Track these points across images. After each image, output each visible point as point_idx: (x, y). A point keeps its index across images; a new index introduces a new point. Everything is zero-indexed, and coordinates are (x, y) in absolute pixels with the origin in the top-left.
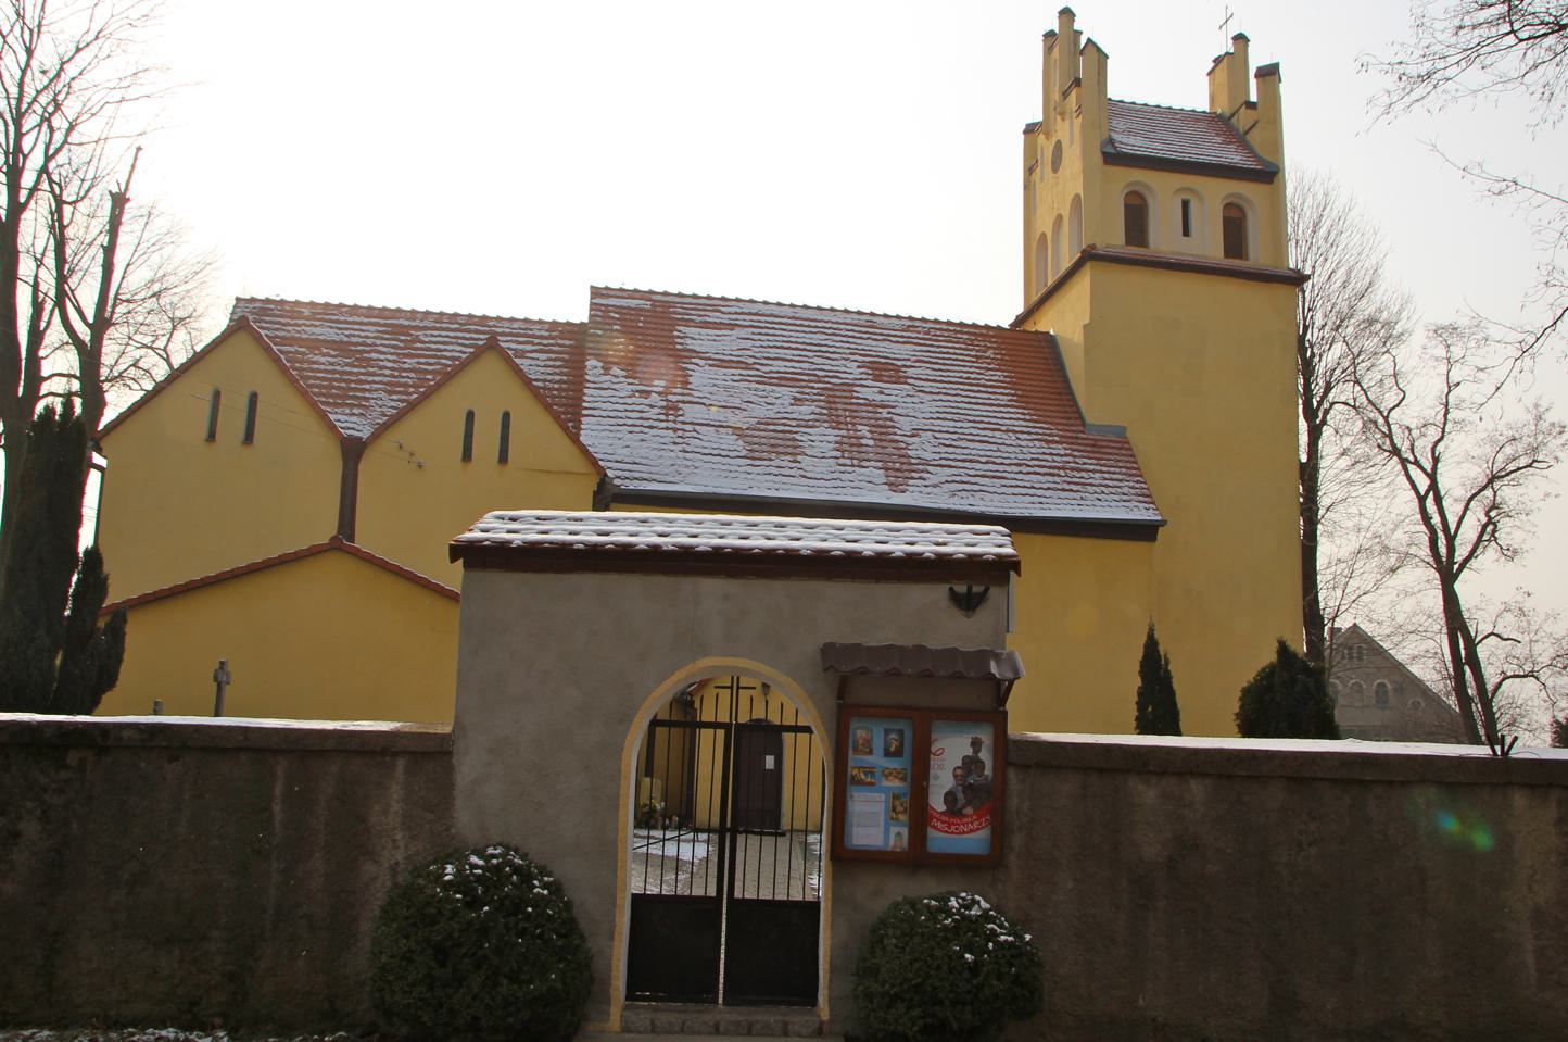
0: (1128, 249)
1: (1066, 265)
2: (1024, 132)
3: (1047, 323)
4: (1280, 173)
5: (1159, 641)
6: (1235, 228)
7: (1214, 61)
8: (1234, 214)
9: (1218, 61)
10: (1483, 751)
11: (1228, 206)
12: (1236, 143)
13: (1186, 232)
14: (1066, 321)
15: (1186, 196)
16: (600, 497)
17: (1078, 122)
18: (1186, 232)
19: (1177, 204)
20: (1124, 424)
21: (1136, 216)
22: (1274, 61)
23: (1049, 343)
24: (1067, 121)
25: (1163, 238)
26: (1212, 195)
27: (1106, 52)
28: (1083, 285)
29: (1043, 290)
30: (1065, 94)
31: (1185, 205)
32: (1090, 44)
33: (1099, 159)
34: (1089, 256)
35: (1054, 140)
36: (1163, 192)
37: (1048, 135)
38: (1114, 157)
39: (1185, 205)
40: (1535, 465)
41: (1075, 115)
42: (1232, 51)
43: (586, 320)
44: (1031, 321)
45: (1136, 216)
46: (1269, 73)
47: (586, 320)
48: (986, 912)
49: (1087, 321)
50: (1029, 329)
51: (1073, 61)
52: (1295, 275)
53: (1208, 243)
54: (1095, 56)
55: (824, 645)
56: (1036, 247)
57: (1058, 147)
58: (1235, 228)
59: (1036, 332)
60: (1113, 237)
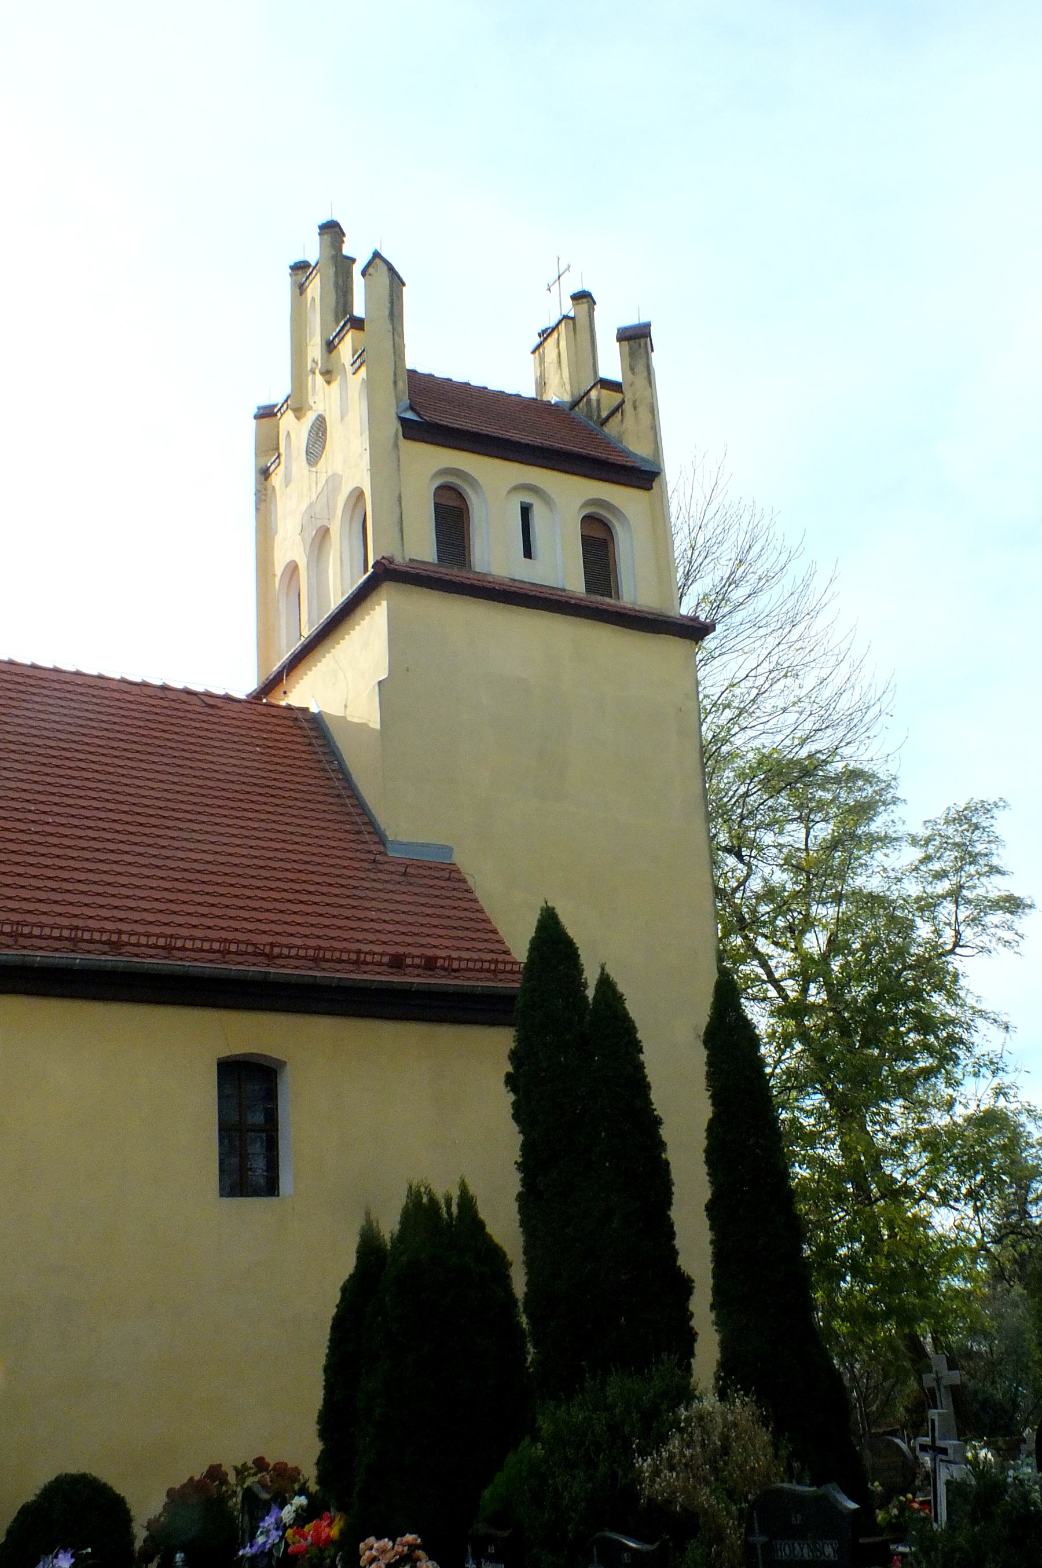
0: (442, 569)
1: (335, 600)
2: (256, 417)
3: (305, 693)
4: (660, 477)
5: (82, 1471)
6: (598, 544)
7: (539, 335)
8: (598, 533)
9: (545, 334)
11: (589, 520)
12: (589, 440)
13: (528, 553)
14: (343, 688)
15: (528, 498)
18: (528, 553)
19: (526, 485)
20: (450, 844)
21: (452, 516)
22: (644, 320)
23: (312, 728)
24: (335, 385)
25: (493, 553)
26: (568, 496)
27: (404, 280)
28: (374, 623)
29: (297, 646)
30: (330, 346)
31: (526, 511)
32: (377, 260)
33: (395, 426)
34: (384, 575)
35: (310, 417)
36: (496, 486)
37: (299, 412)
38: (415, 430)
39: (526, 511)
40: (958, 950)
41: (350, 370)
42: (572, 314)
44: (278, 692)
45: (452, 516)
46: (636, 339)
49: (384, 675)
50: (274, 702)
51: (347, 294)
52: (690, 623)
53: (561, 567)
54: (384, 278)
56: (274, 586)
57: (320, 429)
58: (598, 544)
59: (289, 708)
60: (422, 546)
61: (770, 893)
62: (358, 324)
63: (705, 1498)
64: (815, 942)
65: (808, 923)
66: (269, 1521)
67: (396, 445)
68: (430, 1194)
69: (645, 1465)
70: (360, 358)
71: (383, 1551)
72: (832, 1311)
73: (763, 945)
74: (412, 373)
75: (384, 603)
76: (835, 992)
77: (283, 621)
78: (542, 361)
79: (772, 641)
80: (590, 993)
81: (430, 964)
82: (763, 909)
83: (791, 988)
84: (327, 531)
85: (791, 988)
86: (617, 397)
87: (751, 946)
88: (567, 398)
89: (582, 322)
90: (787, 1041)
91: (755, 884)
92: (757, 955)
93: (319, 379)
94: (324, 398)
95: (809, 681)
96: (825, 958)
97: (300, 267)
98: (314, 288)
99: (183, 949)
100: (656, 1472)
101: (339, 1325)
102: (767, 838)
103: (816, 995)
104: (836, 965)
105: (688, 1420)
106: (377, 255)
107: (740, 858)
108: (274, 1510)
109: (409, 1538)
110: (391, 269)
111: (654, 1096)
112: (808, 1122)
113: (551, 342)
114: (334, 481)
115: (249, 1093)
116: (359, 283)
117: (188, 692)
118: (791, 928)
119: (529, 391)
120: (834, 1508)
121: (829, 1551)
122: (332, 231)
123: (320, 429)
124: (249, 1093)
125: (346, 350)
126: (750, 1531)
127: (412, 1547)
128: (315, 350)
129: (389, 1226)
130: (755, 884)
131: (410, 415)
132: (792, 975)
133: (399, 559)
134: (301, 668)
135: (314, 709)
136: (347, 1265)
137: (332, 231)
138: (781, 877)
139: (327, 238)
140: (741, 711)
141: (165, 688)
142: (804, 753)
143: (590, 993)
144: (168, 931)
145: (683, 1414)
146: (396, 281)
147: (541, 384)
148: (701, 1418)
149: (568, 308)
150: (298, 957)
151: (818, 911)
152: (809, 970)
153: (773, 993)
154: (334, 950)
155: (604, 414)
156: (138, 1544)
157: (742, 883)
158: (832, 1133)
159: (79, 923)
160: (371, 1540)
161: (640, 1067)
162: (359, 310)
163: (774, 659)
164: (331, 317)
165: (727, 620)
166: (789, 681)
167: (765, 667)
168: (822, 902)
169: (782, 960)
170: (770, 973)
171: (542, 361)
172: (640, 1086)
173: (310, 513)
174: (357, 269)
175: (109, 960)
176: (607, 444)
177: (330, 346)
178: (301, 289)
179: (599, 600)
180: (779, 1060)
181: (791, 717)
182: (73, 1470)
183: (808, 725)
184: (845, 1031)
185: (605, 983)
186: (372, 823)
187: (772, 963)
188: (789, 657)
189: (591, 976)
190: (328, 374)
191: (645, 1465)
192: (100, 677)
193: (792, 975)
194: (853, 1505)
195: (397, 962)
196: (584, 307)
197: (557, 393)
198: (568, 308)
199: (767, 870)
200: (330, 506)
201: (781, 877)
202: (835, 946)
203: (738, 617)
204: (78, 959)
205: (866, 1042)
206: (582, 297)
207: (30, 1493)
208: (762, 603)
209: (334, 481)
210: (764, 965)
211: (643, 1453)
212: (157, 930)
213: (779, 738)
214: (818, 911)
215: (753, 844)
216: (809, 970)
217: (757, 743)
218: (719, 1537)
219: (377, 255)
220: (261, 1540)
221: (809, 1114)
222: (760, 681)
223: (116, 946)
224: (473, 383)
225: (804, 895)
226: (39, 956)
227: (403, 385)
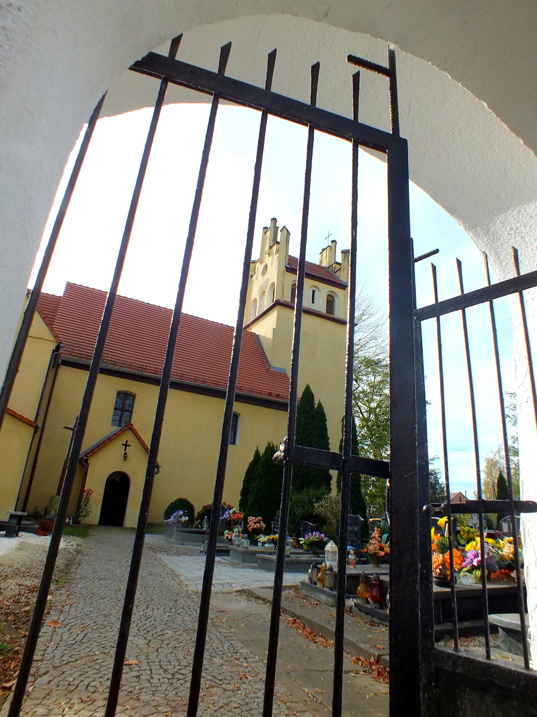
1: (265, 308)
6: (330, 302)
8: (331, 299)
9: (323, 250)
10: (12, 694)
13: (313, 302)
15: (314, 289)
16: (56, 353)
17: (276, 257)
18: (313, 302)
23: (256, 337)
24: (271, 257)
26: (324, 289)
28: (273, 316)
30: (271, 247)
31: (314, 292)
34: (277, 304)
35: (264, 264)
37: (261, 263)
39: (314, 292)
41: (275, 254)
43: (62, 296)
47: (62, 296)
48: (448, 522)
53: (321, 306)
55: (405, 141)
58: (330, 302)
59: (251, 332)
61: (363, 392)
62: (278, 243)
63: (329, 514)
64: (373, 405)
65: (372, 400)
66: (227, 513)
67: (284, 273)
68: (273, 444)
69: (316, 505)
70: (277, 251)
71: (253, 520)
72: (366, 494)
73: (360, 404)
74: (99, 523)
75: (276, 312)
76: (377, 416)
77: (252, 312)
78: (322, 256)
79: (371, 330)
80: (316, 406)
81: (278, 396)
82: (361, 395)
83: (366, 415)
84: (265, 292)
85: (366, 415)
86: (340, 267)
87: (357, 404)
88: (327, 266)
89: (333, 247)
90: (363, 427)
91: (360, 389)
92: (358, 406)
93: (267, 255)
94: (268, 260)
95: (380, 341)
96: (375, 408)
97: (265, 228)
98: (268, 233)
99: (220, 385)
100: (318, 507)
101: (248, 472)
102: (364, 378)
103: (372, 417)
104: (378, 410)
105: (327, 498)
106: (284, 227)
107: (357, 382)
108: (228, 510)
109: (259, 518)
110: (287, 230)
111: (328, 432)
112: (366, 447)
113: (325, 251)
114: (268, 280)
115: (231, 423)
116: (279, 233)
117: (227, 326)
118: (368, 401)
119: (318, 263)
120: (359, 519)
121: (356, 529)
122: (274, 220)
123: (266, 267)
124: (231, 423)
125: (274, 248)
126: (338, 523)
127: (260, 520)
128: (267, 248)
129: (262, 451)
130: (360, 389)
131: (288, 266)
132: (367, 411)
133: (281, 300)
134: (255, 324)
135: (257, 333)
136: (251, 458)
137: (274, 220)
138: (366, 388)
139: (273, 222)
140: (362, 346)
141: (222, 324)
142: (376, 358)
143: (316, 406)
144: (217, 380)
145: (326, 496)
146: (288, 233)
147: (321, 262)
148: (330, 498)
149: (330, 244)
150: (246, 390)
151: (375, 397)
152: (371, 411)
153: (361, 416)
154: (255, 390)
155: (336, 270)
156: (196, 516)
157: (357, 389)
158: (371, 451)
159: (197, 376)
160: (251, 517)
161: (326, 425)
162: (278, 240)
163: (372, 334)
164: (272, 240)
165: (361, 324)
166: (374, 340)
167: (369, 336)
168: (376, 395)
169: (364, 408)
170: (361, 411)
171: (322, 256)
172: (325, 429)
173: (261, 287)
174: (279, 230)
175: (203, 385)
176: (336, 278)
177: (271, 247)
178: (265, 233)
179: (329, 315)
180: (361, 432)
181: (374, 349)
182: (183, 497)
183: (378, 352)
184: (378, 426)
185: (320, 404)
186: (268, 362)
187: (362, 408)
188: (374, 334)
189: (316, 402)
190: (269, 254)
191: (316, 505)
192: (207, 320)
193: (367, 411)
194: (362, 519)
195: (270, 394)
196: (334, 244)
197: (325, 264)
198: (330, 244)
199: (363, 385)
200: (266, 286)
201: (366, 388)
202: (378, 406)
203: (364, 323)
204: (195, 384)
205: (383, 430)
206: (334, 242)
207: (173, 500)
208: (370, 320)
209: (268, 280)
210: (360, 409)
211: (316, 503)
212: (214, 380)
213: (370, 354)
214: (375, 397)
215: (361, 380)
216: (371, 411)
217: (364, 355)
218: (331, 524)
219: (284, 227)
220: (225, 516)
221: (366, 445)
222: (367, 339)
223: (204, 382)
224: (107, 118)
225: (373, 393)
226: (186, 382)
227: (287, 259)
